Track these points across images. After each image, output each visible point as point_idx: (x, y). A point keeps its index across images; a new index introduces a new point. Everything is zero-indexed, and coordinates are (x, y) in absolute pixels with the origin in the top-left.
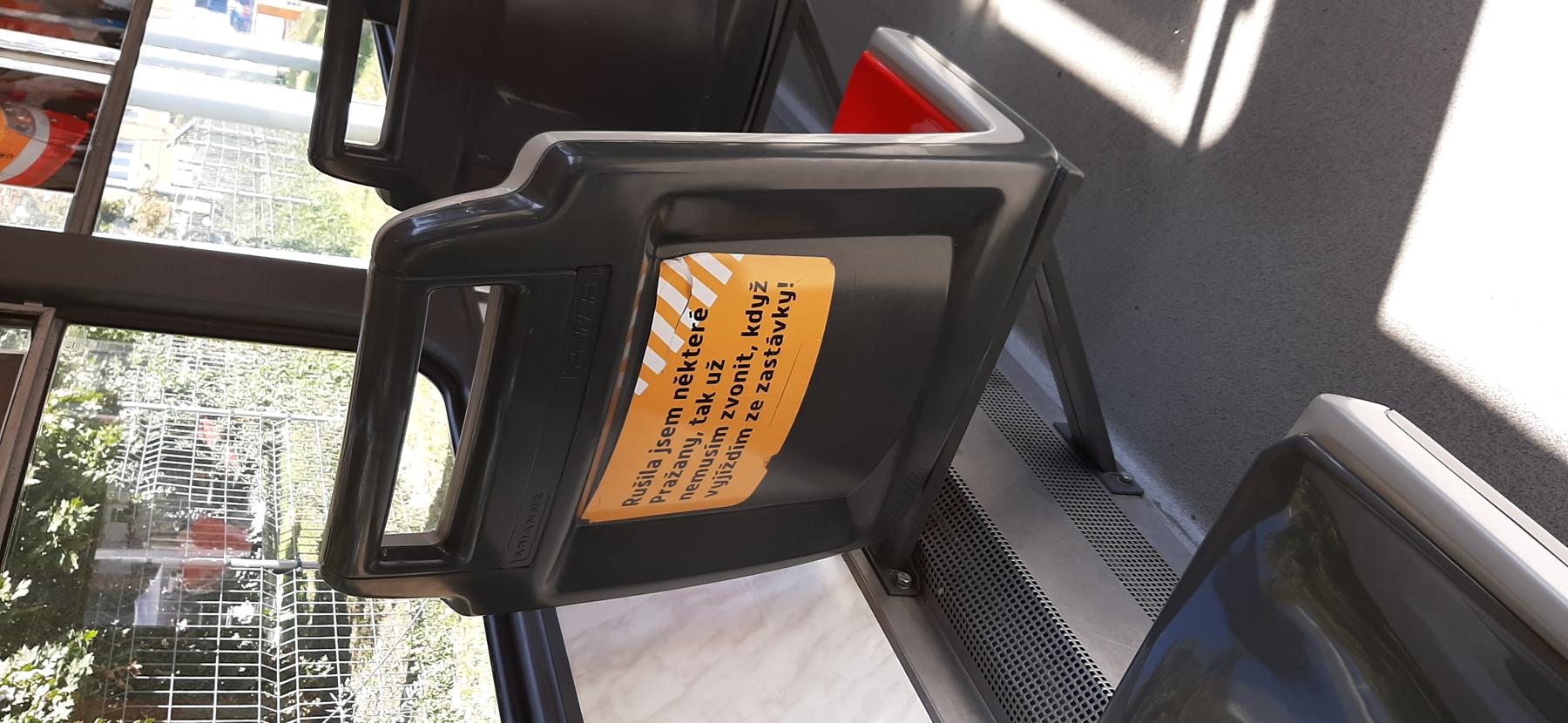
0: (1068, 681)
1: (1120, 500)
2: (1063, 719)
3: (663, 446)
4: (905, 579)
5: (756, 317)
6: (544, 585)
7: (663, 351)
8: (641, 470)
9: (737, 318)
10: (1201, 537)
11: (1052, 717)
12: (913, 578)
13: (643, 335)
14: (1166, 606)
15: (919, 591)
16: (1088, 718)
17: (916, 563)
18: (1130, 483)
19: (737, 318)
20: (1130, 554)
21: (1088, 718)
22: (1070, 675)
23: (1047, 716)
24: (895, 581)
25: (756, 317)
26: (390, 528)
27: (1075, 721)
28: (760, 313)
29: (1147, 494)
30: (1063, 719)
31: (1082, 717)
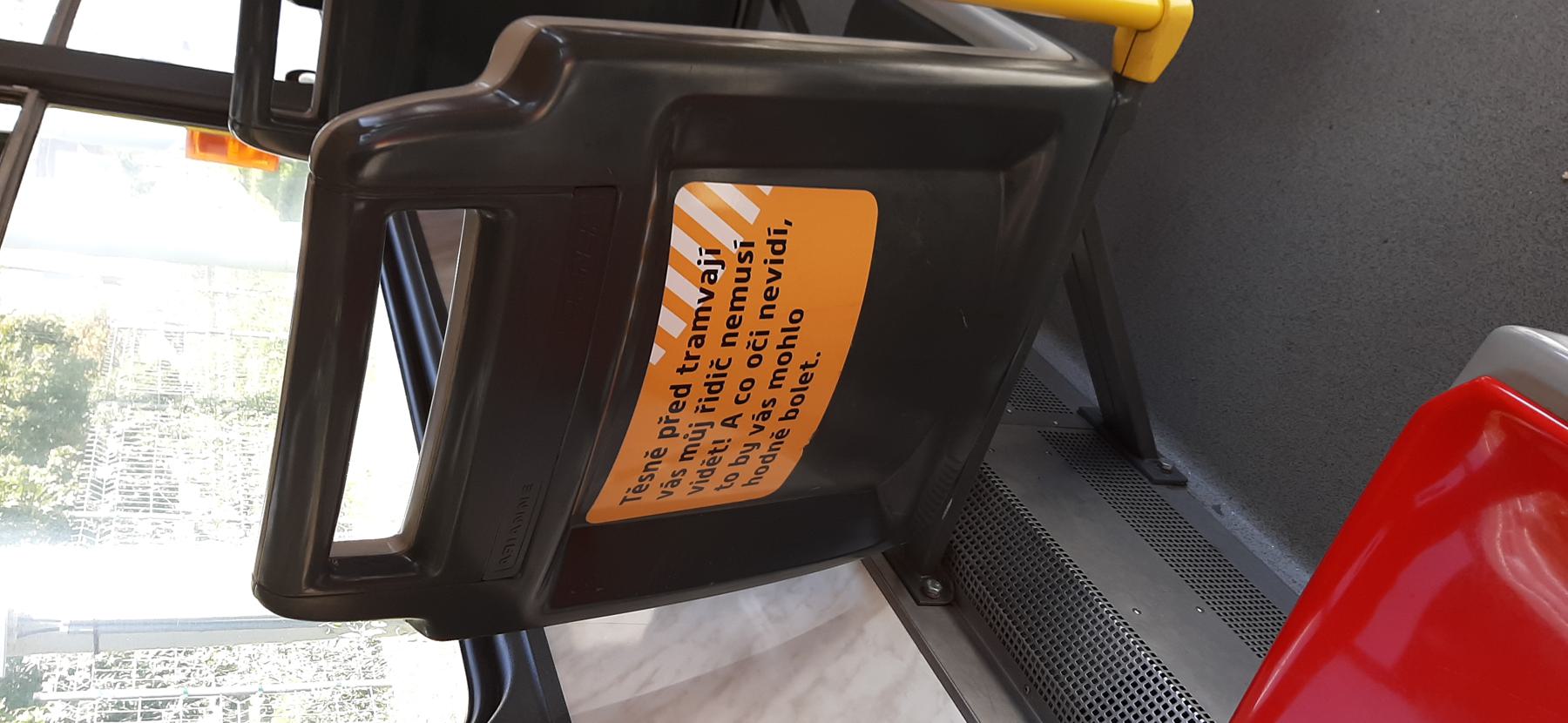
0: (1127, 690)
1: (1161, 490)
2: (1164, 719)
3: (669, 432)
4: (936, 589)
5: (778, 247)
6: (533, 596)
7: (679, 307)
8: (650, 470)
9: (763, 261)
10: (1308, 578)
11: (1123, 715)
12: (945, 585)
13: (655, 293)
14: (1280, 637)
15: (951, 601)
16: (1144, 717)
17: (945, 567)
18: (1173, 471)
19: (763, 261)
20: (1214, 573)
21: (1144, 717)
22: (1142, 686)
23: (1117, 715)
24: (924, 591)
25: (778, 247)
26: (338, 537)
27: (1115, 721)
28: (783, 242)
29: (1191, 486)
30: (1164, 719)
31: (1136, 717)
